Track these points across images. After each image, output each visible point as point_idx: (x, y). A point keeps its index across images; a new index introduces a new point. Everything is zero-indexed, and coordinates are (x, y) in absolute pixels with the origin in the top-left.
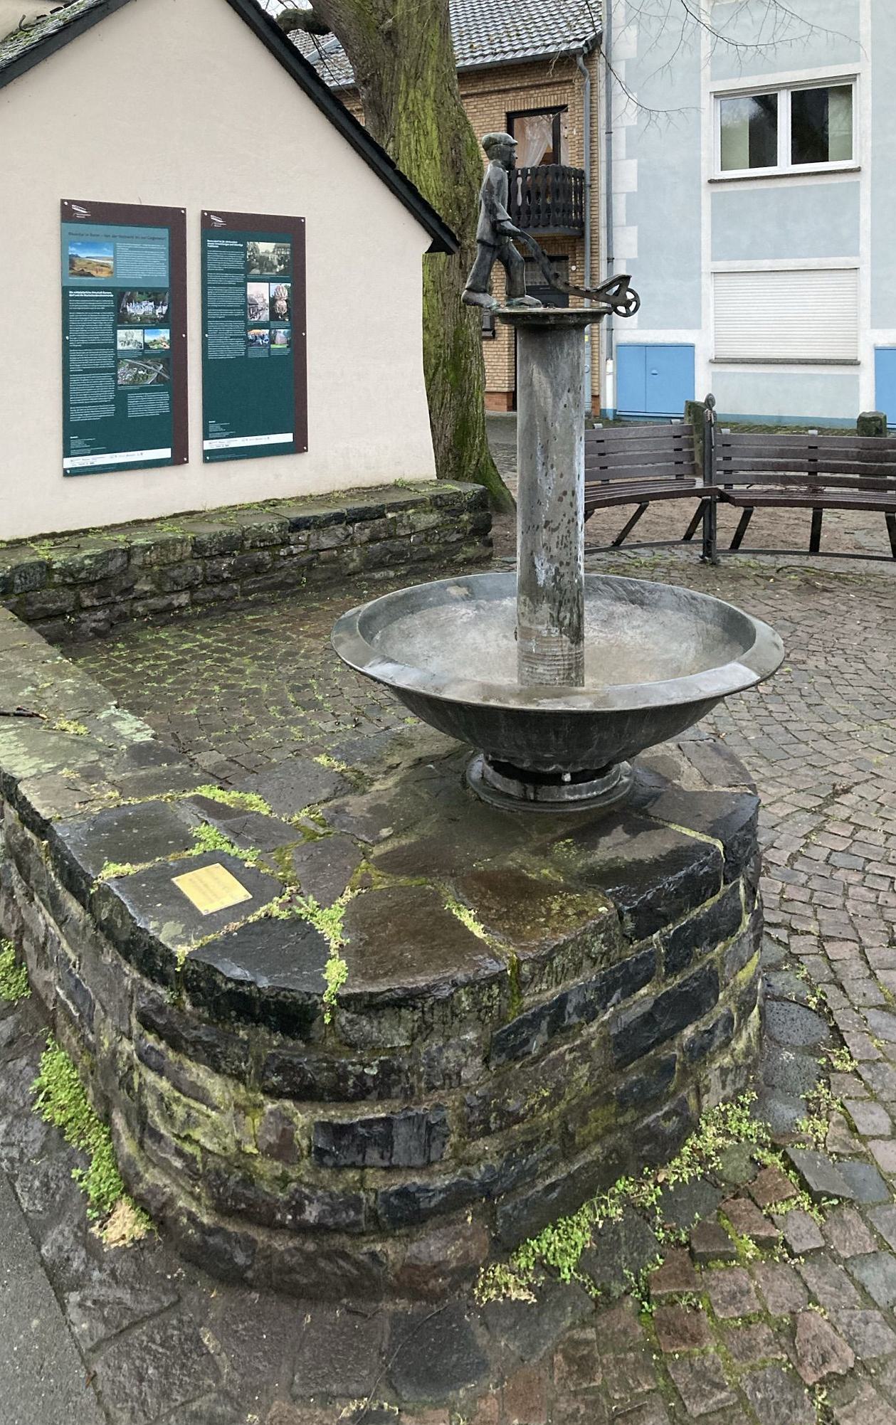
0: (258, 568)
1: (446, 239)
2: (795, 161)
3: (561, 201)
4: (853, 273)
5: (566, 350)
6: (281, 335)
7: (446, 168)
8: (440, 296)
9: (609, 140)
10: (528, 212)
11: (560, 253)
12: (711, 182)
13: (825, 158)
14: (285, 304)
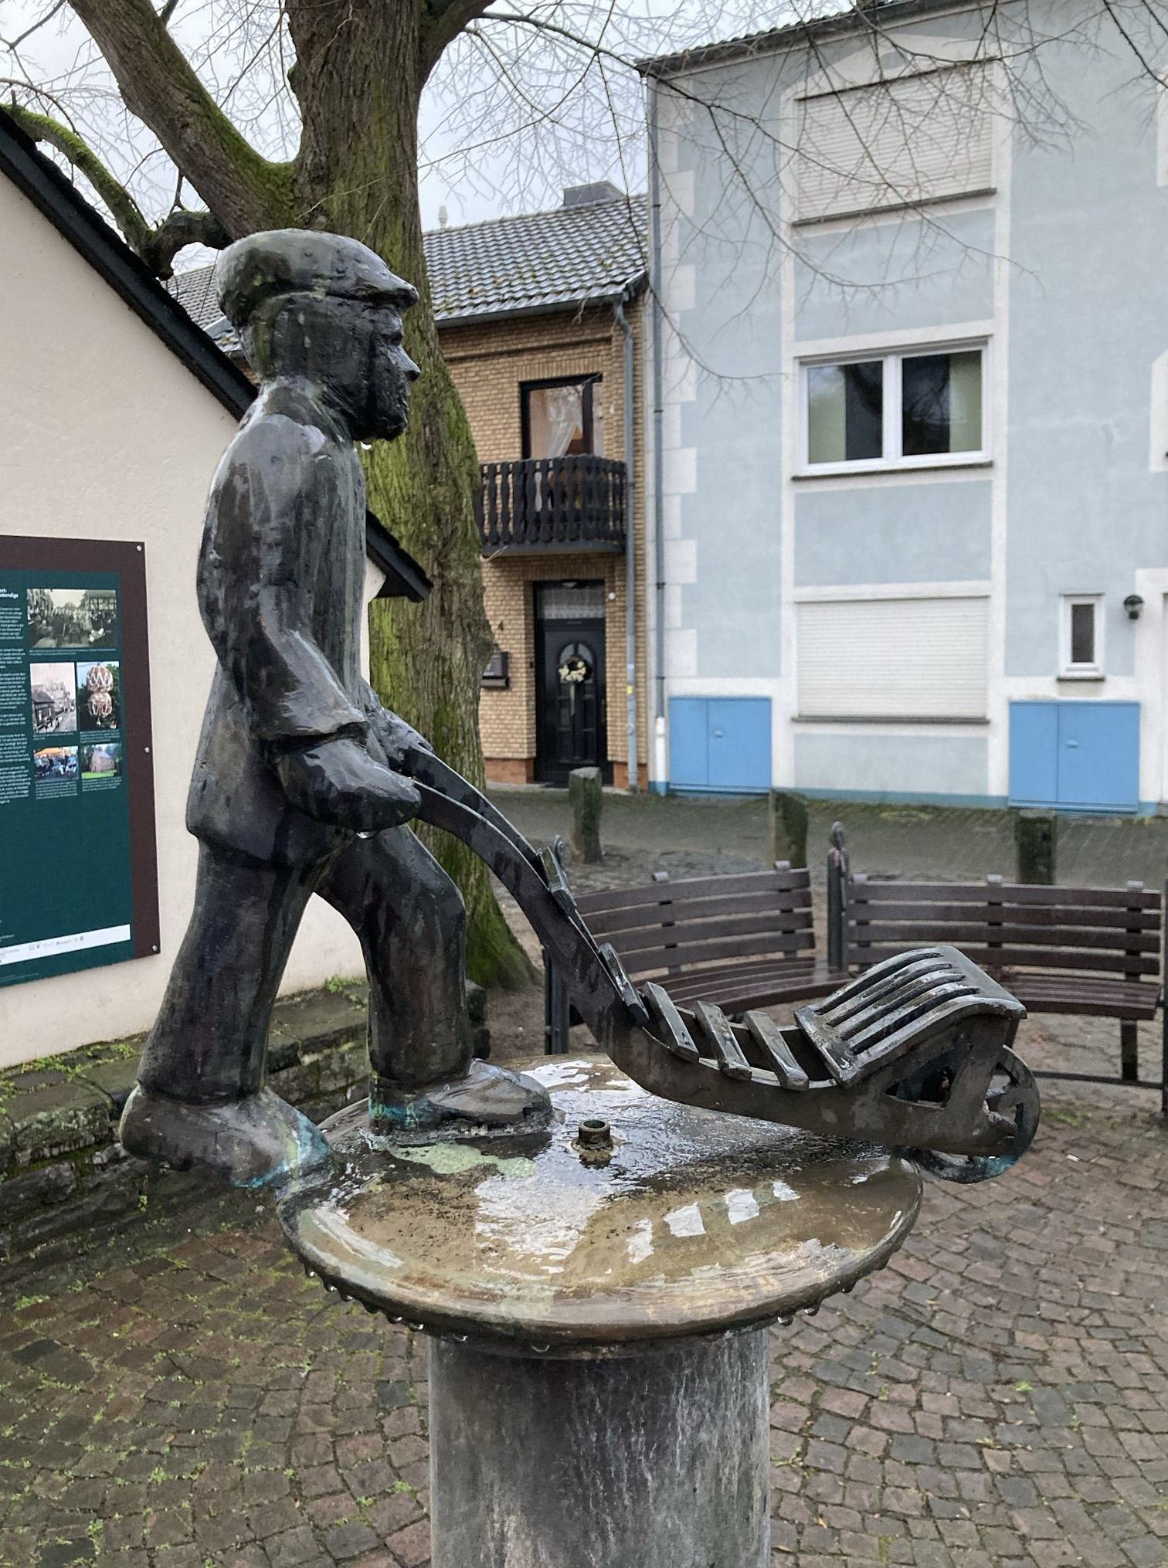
0: (47, 1197)
1: (408, 576)
2: (909, 449)
3: (595, 505)
4: (980, 603)
5: (680, 1443)
6: (103, 755)
7: (415, 455)
8: (409, 659)
9: (658, 422)
10: (551, 520)
11: (592, 575)
12: (796, 479)
13: (947, 451)
14: (109, 698)
